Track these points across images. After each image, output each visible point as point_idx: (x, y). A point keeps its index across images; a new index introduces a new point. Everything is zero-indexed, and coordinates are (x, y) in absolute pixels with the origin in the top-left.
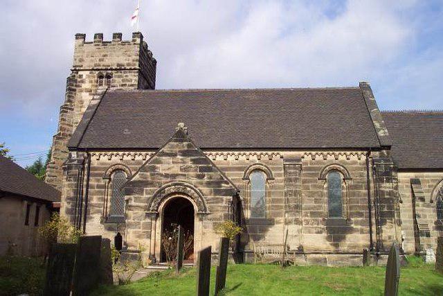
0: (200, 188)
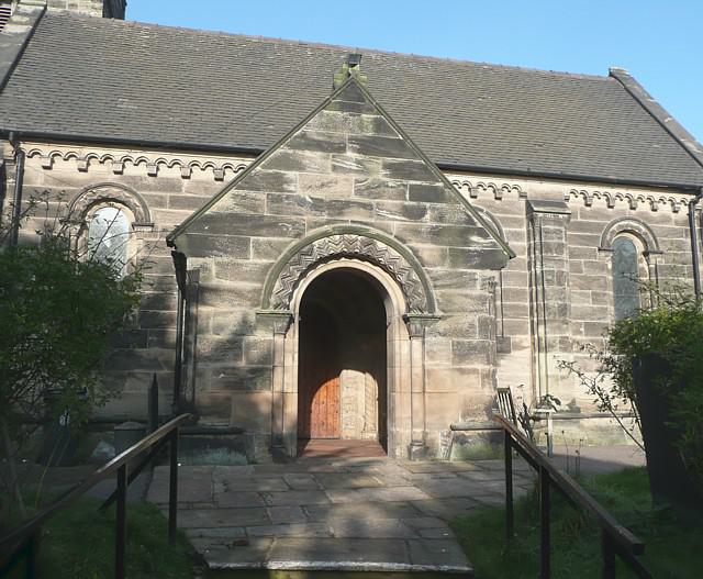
0: (413, 244)
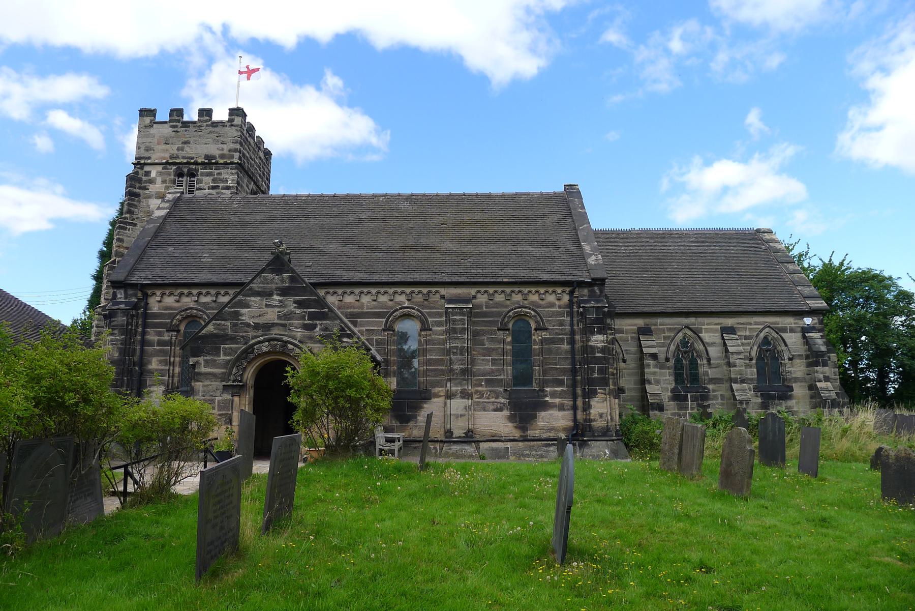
0: (309, 345)
